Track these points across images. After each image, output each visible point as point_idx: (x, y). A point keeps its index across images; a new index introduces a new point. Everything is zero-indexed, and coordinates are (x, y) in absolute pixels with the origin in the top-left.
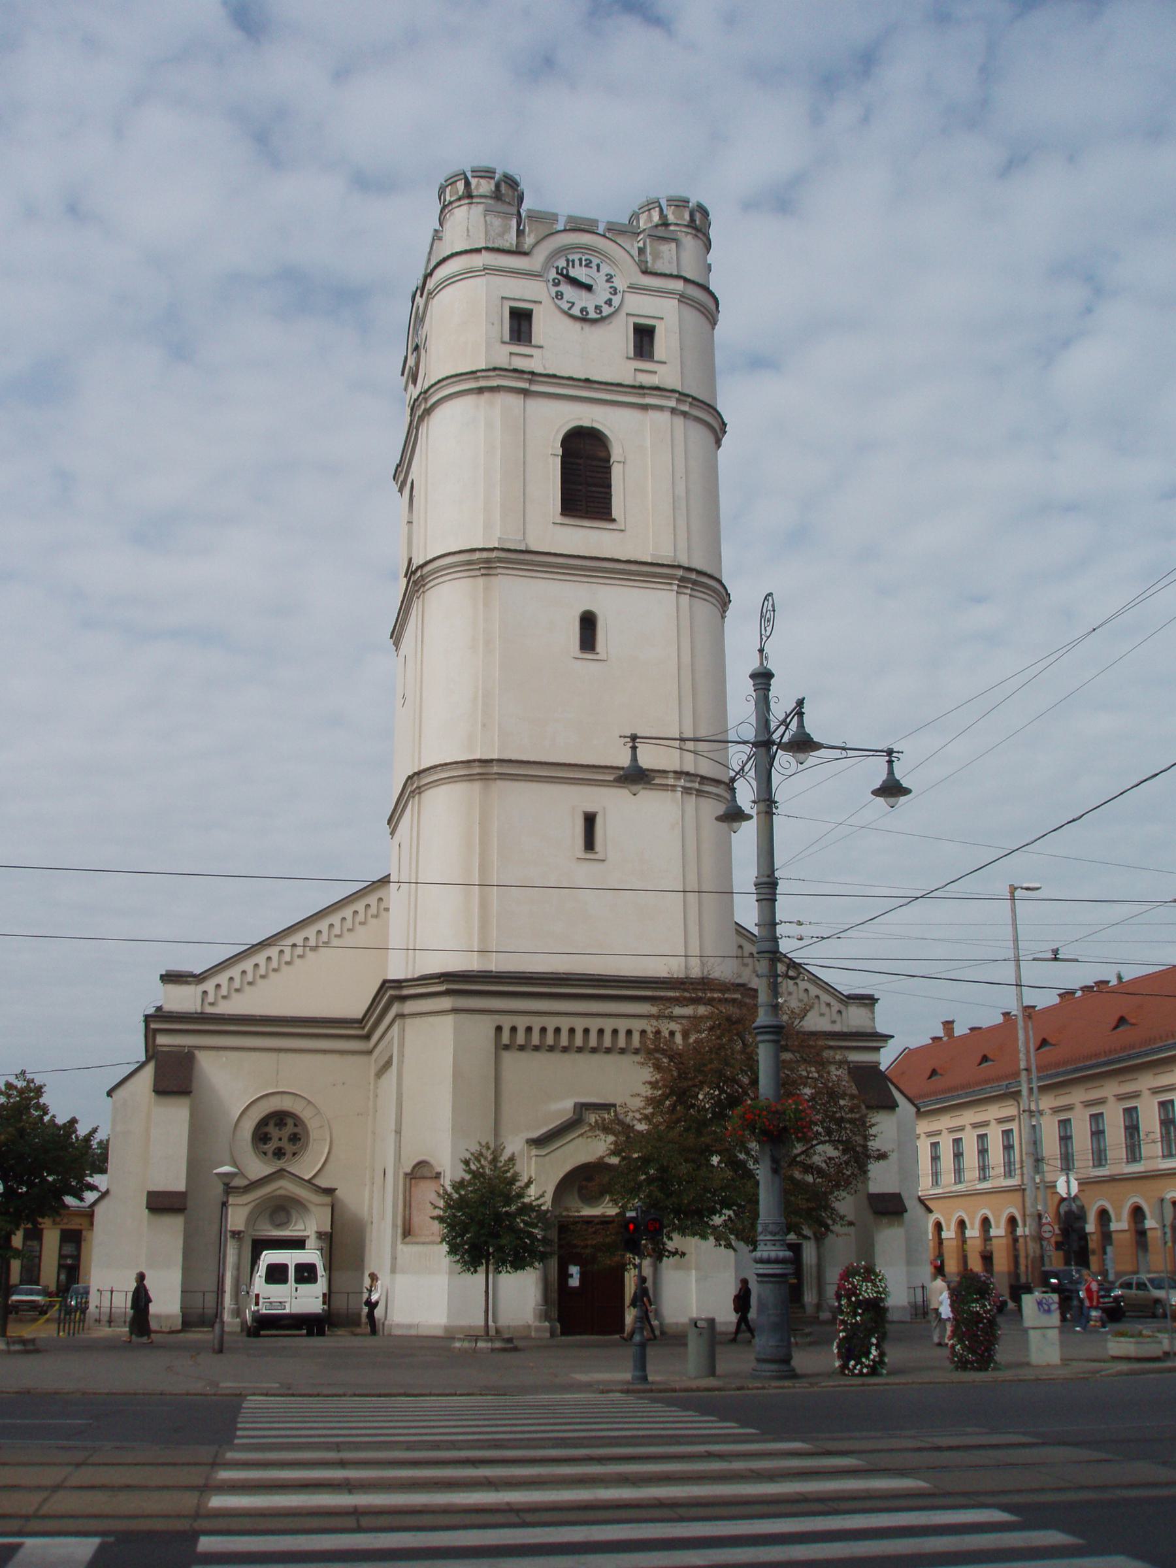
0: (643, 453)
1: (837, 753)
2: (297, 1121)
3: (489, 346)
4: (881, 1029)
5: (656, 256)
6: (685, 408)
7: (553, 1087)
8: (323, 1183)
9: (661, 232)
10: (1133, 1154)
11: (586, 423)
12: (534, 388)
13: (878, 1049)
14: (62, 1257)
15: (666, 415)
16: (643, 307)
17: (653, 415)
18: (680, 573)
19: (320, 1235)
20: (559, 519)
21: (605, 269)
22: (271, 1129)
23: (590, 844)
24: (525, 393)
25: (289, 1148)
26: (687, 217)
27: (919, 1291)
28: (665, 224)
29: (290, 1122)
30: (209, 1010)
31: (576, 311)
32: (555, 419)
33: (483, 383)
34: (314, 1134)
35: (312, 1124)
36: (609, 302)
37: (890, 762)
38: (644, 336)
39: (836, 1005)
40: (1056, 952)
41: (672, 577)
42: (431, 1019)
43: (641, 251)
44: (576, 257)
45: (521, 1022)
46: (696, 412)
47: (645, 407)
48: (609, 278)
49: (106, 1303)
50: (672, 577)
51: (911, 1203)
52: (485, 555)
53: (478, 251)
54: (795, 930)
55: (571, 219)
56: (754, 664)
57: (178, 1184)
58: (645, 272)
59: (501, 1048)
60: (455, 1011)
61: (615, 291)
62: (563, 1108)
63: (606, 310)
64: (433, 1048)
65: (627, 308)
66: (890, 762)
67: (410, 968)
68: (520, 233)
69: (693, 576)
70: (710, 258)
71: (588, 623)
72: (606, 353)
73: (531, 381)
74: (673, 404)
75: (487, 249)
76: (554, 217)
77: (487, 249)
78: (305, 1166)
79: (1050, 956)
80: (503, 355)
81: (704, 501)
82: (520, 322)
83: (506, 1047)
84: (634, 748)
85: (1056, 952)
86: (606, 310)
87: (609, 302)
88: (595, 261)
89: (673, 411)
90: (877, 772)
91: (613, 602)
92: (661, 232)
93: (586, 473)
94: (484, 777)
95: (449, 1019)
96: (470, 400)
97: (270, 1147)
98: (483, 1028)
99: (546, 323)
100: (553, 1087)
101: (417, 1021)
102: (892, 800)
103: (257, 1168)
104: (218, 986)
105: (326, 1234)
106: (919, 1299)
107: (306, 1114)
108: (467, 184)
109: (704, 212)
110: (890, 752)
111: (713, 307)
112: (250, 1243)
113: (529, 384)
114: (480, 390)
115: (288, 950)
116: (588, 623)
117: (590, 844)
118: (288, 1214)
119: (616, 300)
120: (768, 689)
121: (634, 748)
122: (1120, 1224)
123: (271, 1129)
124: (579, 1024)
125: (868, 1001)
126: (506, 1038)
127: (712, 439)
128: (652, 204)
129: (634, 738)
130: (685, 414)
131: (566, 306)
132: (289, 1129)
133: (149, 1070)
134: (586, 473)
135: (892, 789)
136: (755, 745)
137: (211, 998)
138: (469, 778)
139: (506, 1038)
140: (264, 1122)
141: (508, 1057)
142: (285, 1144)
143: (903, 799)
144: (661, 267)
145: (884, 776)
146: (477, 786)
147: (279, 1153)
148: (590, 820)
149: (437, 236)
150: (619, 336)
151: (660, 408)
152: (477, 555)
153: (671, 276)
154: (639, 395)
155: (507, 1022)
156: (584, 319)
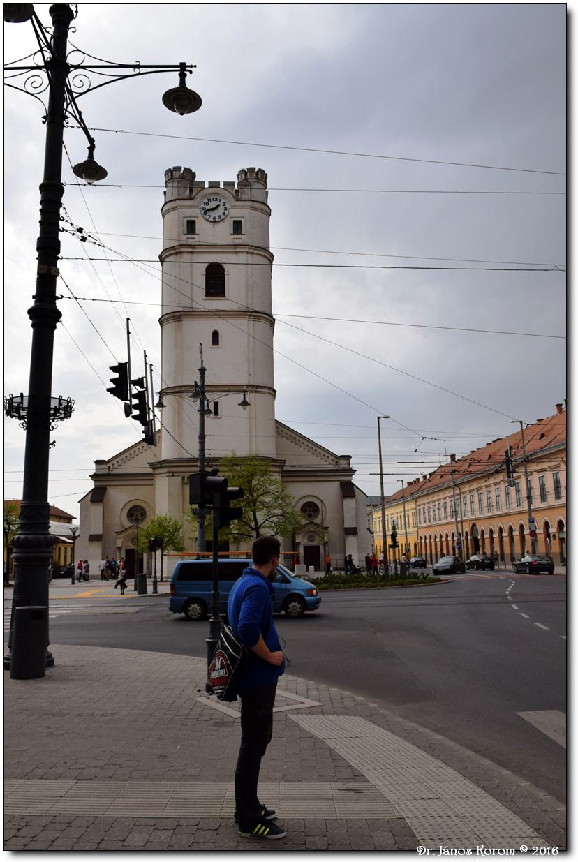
2: (143, 509)
3: (179, 236)
6: (252, 251)
11: (215, 261)
12: (195, 250)
14: (530, 573)
16: (236, 213)
17: (240, 255)
20: (204, 298)
21: (222, 201)
24: (192, 252)
26: (255, 175)
29: (131, 512)
31: (211, 219)
33: (177, 251)
36: (224, 214)
39: (335, 460)
44: (211, 198)
46: (256, 252)
47: (237, 253)
48: (224, 204)
52: (178, 314)
53: (175, 200)
54: (209, 452)
55: (210, 183)
56: (200, 366)
57: (100, 532)
58: (237, 200)
61: (226, 209)
63: (217, 219)
65: (230, 216)
67: (254, 447)
68: (191, 191)
69: (254, 314)
71: (216, 336)
72: (223, 234)
73: (192, 248)
74: (247, 250)
80: (185, 239)
82: (191, 227)
86: (223, 217)
87: (224, 214)
88: (219, 198)
89: (247, 253)
91: (221, 325)
93: (215, 281)
97: (134, 518)
99: (201, 225)
102: (244, 407)
103: (304, 522)
104: (114, 464)
108: (172, 174)
111: (268, 210)
112: (124, 551)
114: (176, 253)
115: (141, 449)
116: (216, 336)
119: (226, 212)
120: (204, 373)
125: (348, 458)
130: (252, 253)
133: (91, 494)
134: (215, 281)
142: (135, 517)
143: (248, 407)
144: (245, 197)
147: (137, 520)
150: (227, 226)
151: (243, 252)
153: (248, 200)
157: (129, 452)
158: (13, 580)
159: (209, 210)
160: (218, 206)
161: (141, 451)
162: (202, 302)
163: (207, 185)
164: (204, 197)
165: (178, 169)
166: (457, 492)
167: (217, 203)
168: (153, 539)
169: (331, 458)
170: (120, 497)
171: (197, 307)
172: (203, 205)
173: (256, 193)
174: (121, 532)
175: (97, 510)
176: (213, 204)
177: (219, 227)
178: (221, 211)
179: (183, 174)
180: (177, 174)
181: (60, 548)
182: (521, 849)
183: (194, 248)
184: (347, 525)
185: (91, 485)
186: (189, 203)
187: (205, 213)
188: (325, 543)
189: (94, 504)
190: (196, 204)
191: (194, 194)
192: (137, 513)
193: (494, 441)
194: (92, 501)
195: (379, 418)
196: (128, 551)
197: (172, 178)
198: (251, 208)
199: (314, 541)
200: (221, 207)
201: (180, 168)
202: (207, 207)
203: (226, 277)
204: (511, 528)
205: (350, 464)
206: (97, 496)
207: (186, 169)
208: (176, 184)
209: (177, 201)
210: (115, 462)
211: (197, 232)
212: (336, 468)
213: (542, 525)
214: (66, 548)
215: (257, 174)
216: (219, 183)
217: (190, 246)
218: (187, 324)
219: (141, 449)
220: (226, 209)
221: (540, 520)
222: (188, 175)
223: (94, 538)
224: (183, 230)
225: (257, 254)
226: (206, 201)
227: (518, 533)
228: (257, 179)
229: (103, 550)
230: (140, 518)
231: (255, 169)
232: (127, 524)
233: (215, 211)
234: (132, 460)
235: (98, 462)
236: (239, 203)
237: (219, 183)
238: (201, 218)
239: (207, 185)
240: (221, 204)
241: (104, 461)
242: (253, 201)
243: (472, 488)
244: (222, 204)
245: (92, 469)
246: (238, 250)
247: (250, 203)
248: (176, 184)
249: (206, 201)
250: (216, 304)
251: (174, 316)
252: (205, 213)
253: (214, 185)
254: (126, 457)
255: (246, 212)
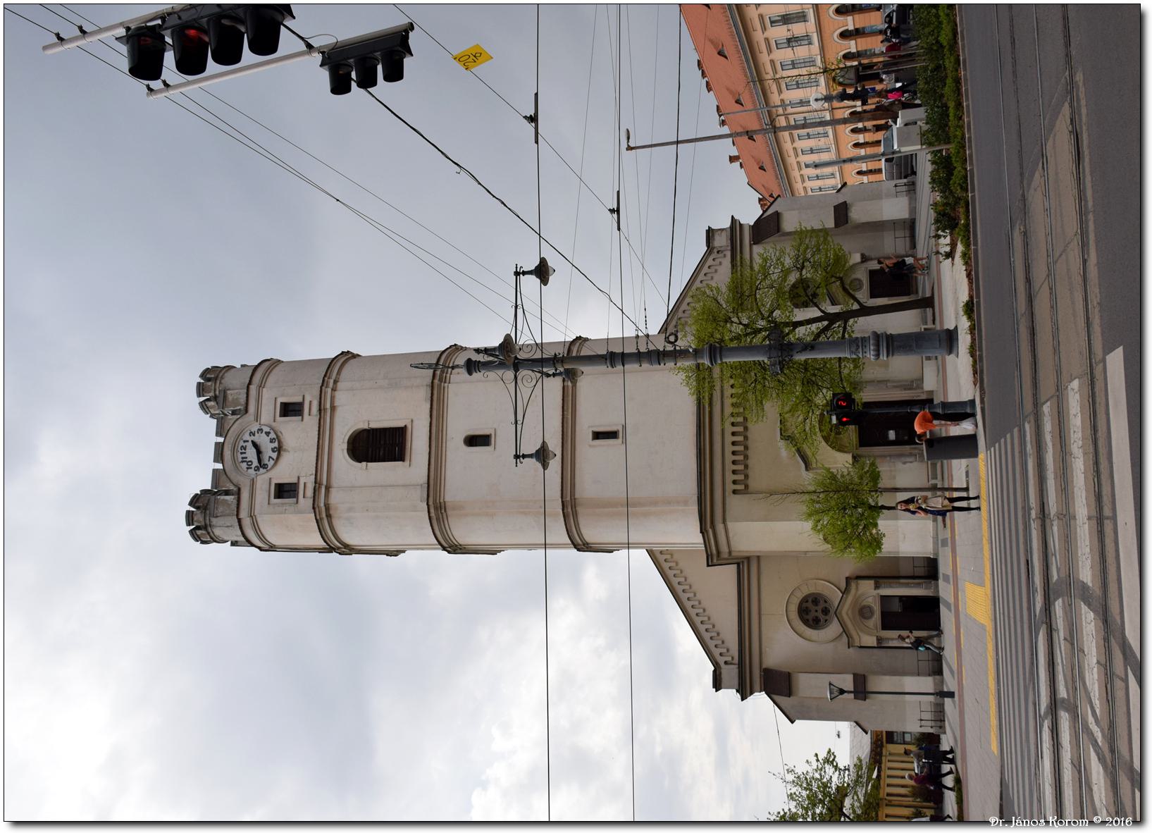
0: (359, 410)
1: (520, 311)
3: (300, 512)
4: (727, 224)
5: (236, 402)
6: (331, 381)
7: (771, 455)
8: (843, 585)
9: (221, 399)
10: (807, 39)
11: (345, 446)
13: (741, 225)
15: (337, 394)
16: (268, 411)
18: (436, 381)
19: (877, 587)
20: (407, 463)
21: (246, 437)
22: (810, 617)
23: (612, 435)
24: (328, 488)
25: (822, 605)
27: (899, 189)
28: (215, 398)
29: (805, 605)
30: (736, 660)
32: (344, 467)
33: (324, 515)
34: (812, 590)
35: (806, 591)
37: (524, 273)
38: (290, 410)
40: (612, 211)
41: (439, 386)
42: (731, 535)
43: (234, 413)
44: (240, 456)
45: (730, 477)
46: (334, 376)
47: (333, 408)
48: (252, 434)
49: (929, 723)
50: (439, 386)
51: (841, 199)
52: (432, 510)
53: (239, 521)
55: (215, 461)
58: (246, 411)
59: (746, 490)
60: (724, 521)
61: (260, 430)
62: (784, 451)
64: (752, 532)
66: (524, 273)
68: (227, 493)
70: (238, 366)
71: (472, 441)
72: (299, 434)
74: (329, 390)
75: (237, 515)
76: (215, 471)
77: (237, 515)
78: (835, 595)
79: (615, 215)
80: (305, 502)
81: (388, 367)
82: (285, 491)
83: (747, 486)
84: (524, 456)
85: (612, 211)
86: (273, 435)
87: (268, 434)
88: (242, 443)
89: (334, 390)
90: (531, 282)
91: (457, 428)
92: (221, 399)
93: (379, 445)
94: (574, 506)
95: (730, 525)
96: (336, 523)
98: (735, 503)
99: (283, 473)
100: (771, 455)
101: (732, 543)
104: (721, 654)
105: (904, 221)
106: (904, 188)
107: (800, 596)
109: (207, 371)
110: (517, 274)
111: (267, 364)
113: (322, 486)
114: (329, 516)
115: (701, 619)
116: (472, 441)
117: (612, 435)
118: (864, 607)
121: (524, 456)
122: (852, 46)
123: (810, 617)
124: (729, 429)
125: (710, 233)
126: (740, 487)
127: (352, 361)
128: (203, 405)
129: (517, 457)
130: (335, 382)
131: (272, 462)
132: (809, 604)
133: (775, 697)
134: (379, 445)
135: (542, 272)
136: (516, 370)
137: (729, 659)
138: (575, 515)
139: (740, 487)
140: (806, 622)
141: (753, 484)
142: (819, 608)
144: (243, 400)
145: (533, 278)
146: (580, 510)
148: (597, 435)
149: (234, 544)
151: (333, 398)
152: (433, 514)
154: (326, 412)
155: (730, 487)
156: (279, 450)
157: (694, 616)
158: (897, 435)
159: (260, 460)
160: (255, 445)
161: (673, 564)
162: (415, 468)
163: (219, 466)
164: (237, 468)
165: (190, 516)
166: (780, 111)
167: (249, 445)
168: (834, 418)
169: (710, 262)
170: (783, 642)
171: (423, 478)
172: (252, 471)
173: (234, 384)
174: (849, 636)
175: (810, 686)
176: (251, 454)
177: (289, 440)
178: (263, 440)
179: (198, 508)
180: (199, 517)
181: (888, 795)
182: (1095, 819)
183: (320, 484)
184: (830, 223)
185: (761, 700)
186: (245, 495)
187: (265, 466)
188: (865, 259)
189: (794, 689)
190: (248, 483)
191: (232, 487)
192: (812, 612)
193: (704, 75)
194: (789, 694)
195: (629, 148)
196: (886, 626)
197: (205, 528)
198: (261, 386)
199: (860, 280)
200: (256, 439)
201: (188, 512)
202: (256, 463)
203: (374, 425)
204: (845, 35)
205: (722, 230)
206: (778, 685)
207: (191, 504)
208: (214, 521)
209: (241, 516)
210: (716, 652)
211: (294, 480)
212: (728, 254)
213: (855, 136)
214: (889, 777)
215: (209, 380)
216: (217, 444)
217: (316, 491)
218: (452, 493)
219: (701, 619)
220: (260, 430)
221: (850, 152)
222: (202, 503)
223: (861, 690)
224: (290, 504)
225: (339, 373)
226: (244, 465)
227: (853, 42)
228: (216, 379)
229: (885, 674)
230: (822, 605)
231: (199, 384)
232: (833, 629)
233: (263, 449)
234: (704, 604)
235: (717, 685)
236: (252, 408)
237: (217, 444)
238: (272, 474)
239: (219, 466)
240: (250, 439)
241: (715, 672)
242: (250, 383)
243: (791, 153)
244: (252, 438)
245: (730, 695)
246: (328, 406)
247: (253, 388)
248: (214, 521)
249: (244, 465)
250: (418, 444)
251: (438, 519)
252: (265, 466)
253: (219, 455)
254: (721, 654)
255: (267, 394)
